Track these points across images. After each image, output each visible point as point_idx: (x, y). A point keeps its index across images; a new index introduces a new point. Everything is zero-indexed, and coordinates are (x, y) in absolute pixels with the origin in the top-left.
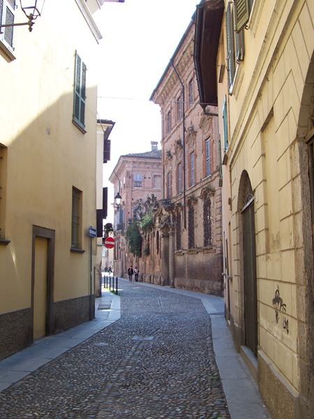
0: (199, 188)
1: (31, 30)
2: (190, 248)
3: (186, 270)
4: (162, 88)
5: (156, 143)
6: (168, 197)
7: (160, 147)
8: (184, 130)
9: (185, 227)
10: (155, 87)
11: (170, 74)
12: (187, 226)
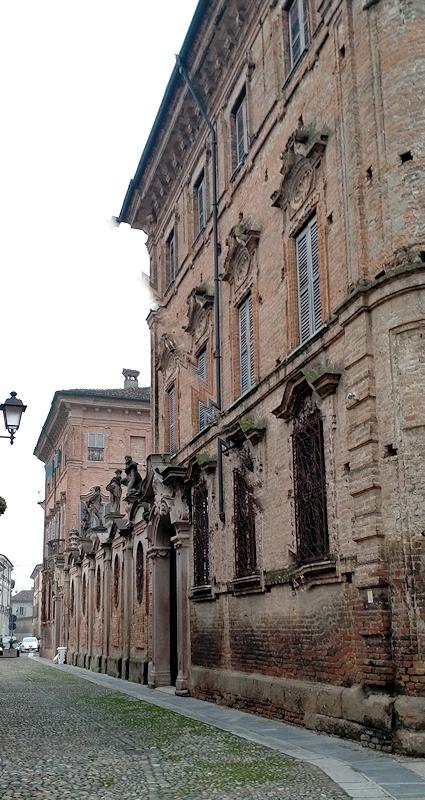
0: (278, 386)
1: (12, 443)
2: (239, 574)
3: (226, 631)
4: (152, 172)
5: (135, 374)
6: (167, 448)
7: (145, 381)
8: (218, 250)
9: (223, 518)
10: (131, 173)
11: (175, 116)
12: (230, 513)
